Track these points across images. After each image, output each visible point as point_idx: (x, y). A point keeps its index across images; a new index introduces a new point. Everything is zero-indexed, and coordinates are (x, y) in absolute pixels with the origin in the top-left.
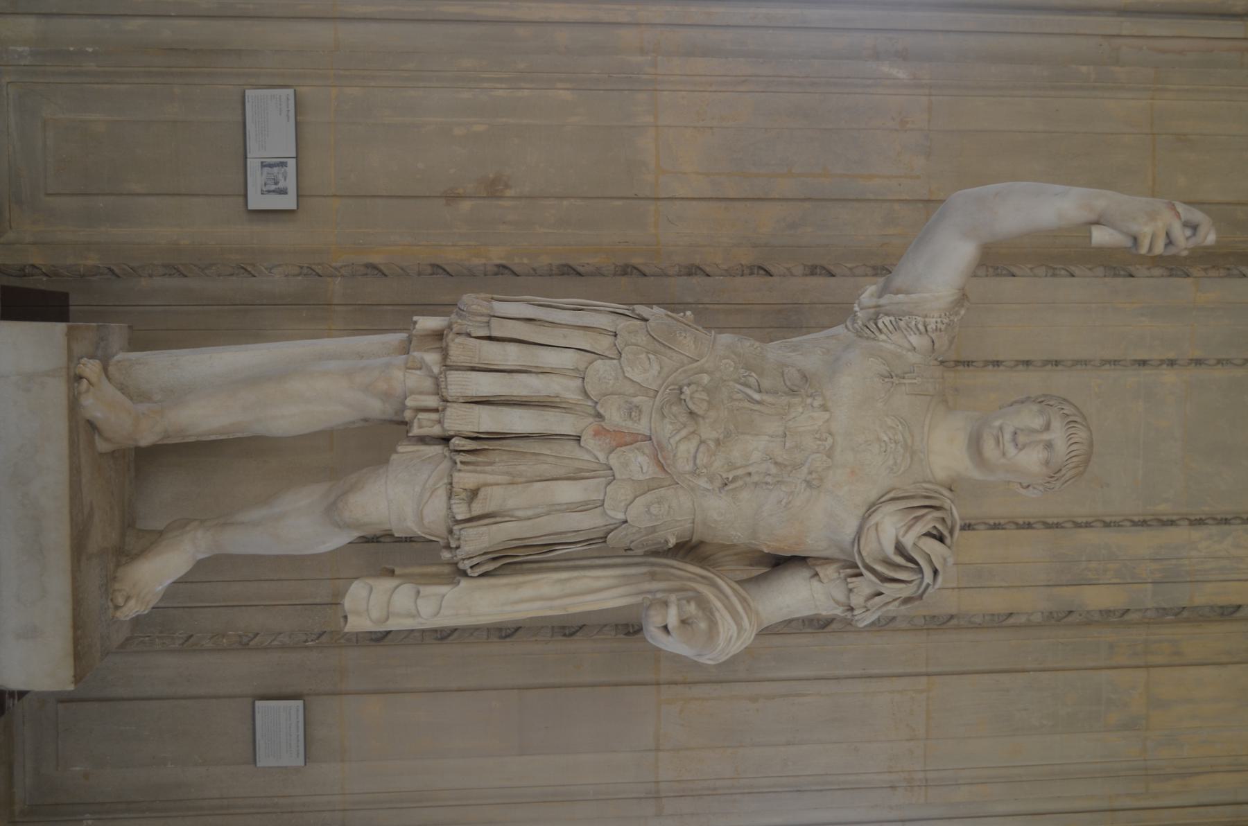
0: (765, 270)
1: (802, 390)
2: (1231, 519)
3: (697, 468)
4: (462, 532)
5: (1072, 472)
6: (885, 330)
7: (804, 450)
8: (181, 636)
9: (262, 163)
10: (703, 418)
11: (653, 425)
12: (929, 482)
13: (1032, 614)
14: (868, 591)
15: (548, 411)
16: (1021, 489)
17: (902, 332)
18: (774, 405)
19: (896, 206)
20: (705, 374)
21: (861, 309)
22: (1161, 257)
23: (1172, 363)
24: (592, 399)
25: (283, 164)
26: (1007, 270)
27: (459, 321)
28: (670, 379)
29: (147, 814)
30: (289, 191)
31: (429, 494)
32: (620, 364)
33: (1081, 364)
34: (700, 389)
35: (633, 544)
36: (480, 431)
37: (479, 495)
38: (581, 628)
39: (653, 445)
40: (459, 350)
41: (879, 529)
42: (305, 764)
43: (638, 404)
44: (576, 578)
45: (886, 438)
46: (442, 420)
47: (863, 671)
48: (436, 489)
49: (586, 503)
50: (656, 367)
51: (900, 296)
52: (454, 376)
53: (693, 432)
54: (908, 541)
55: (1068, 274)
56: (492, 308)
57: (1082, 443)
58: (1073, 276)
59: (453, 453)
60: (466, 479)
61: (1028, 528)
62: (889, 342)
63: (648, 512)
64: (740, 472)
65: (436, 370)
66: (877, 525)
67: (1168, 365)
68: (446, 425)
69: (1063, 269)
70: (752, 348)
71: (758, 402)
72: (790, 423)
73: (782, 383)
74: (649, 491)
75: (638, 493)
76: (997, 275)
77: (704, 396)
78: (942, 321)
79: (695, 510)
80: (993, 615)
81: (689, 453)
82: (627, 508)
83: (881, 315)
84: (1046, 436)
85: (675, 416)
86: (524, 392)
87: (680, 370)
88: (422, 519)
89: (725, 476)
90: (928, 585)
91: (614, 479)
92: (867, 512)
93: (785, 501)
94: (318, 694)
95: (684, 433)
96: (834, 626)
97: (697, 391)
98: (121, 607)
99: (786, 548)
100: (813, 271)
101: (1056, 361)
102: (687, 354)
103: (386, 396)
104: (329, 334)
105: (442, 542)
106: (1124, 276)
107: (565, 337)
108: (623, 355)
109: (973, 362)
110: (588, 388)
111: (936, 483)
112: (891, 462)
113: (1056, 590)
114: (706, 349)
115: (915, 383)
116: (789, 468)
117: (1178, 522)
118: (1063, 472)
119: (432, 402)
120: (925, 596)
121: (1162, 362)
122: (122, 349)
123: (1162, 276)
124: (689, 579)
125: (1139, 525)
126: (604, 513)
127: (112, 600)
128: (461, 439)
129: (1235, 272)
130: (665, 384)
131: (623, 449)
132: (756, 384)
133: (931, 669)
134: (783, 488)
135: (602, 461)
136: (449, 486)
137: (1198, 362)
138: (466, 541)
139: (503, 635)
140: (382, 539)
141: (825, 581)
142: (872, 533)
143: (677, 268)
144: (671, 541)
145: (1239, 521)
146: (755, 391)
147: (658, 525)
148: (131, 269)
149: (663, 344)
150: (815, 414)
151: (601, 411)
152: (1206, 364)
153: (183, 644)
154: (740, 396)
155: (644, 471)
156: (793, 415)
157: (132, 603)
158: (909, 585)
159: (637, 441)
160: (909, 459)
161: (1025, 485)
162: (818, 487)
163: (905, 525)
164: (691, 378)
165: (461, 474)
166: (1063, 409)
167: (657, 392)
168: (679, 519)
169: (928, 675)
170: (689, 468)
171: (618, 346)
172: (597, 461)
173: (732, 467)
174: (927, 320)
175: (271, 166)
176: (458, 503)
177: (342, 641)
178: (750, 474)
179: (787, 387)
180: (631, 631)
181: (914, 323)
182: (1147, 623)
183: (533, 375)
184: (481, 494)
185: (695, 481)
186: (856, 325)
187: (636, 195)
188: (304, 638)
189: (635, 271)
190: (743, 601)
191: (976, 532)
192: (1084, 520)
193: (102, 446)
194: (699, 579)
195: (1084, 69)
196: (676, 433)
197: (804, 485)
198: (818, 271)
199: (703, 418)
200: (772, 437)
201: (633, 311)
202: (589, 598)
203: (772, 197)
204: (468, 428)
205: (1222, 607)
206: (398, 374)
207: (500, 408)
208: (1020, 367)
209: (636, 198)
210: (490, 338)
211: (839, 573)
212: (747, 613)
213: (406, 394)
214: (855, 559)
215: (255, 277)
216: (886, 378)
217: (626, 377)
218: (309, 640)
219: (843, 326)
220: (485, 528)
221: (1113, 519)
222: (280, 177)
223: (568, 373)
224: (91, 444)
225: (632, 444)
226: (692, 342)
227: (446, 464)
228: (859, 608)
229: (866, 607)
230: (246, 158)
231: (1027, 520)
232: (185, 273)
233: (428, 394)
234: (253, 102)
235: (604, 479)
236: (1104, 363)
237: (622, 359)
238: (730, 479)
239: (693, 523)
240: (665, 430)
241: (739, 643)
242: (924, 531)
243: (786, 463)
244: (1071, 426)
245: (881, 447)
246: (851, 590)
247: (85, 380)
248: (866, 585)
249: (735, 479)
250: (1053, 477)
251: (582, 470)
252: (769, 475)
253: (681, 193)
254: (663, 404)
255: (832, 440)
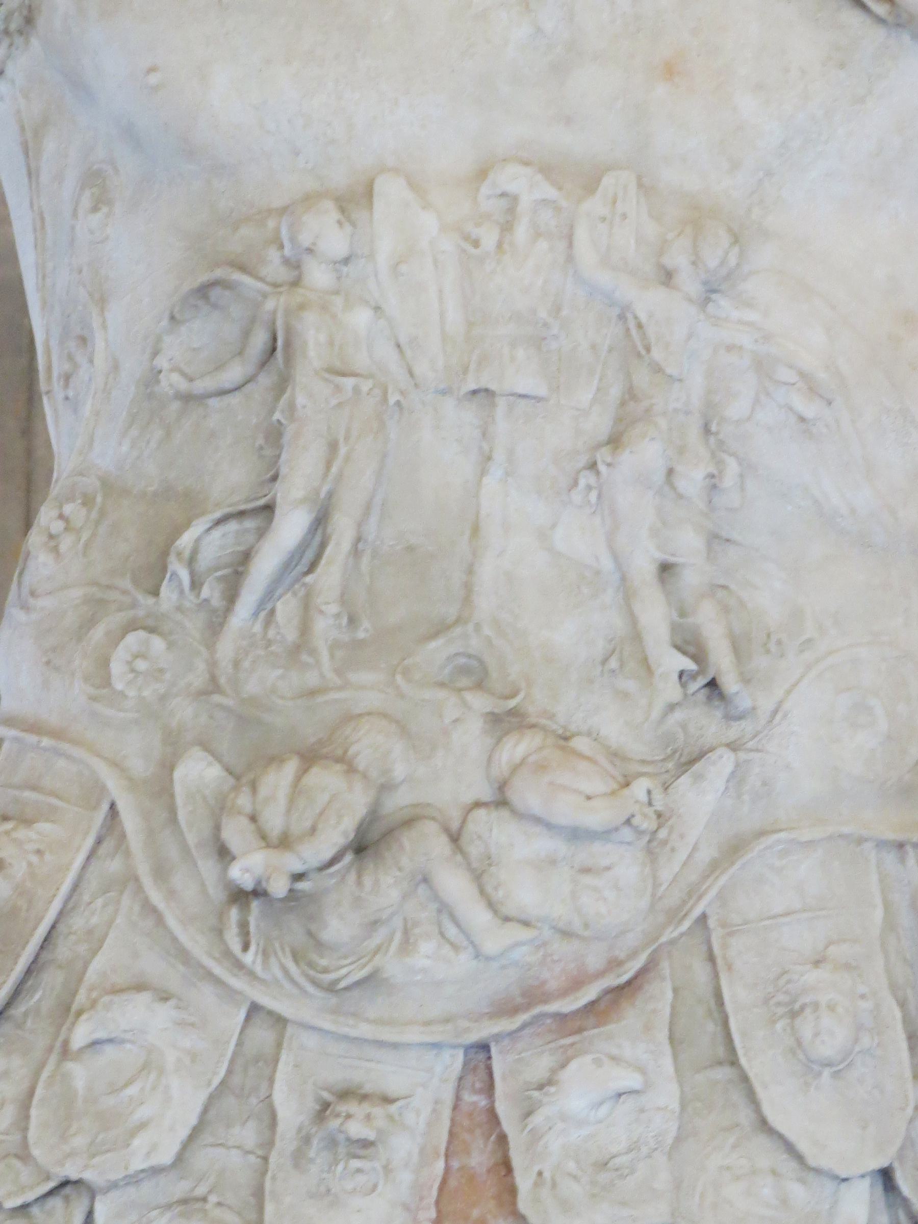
1: (270, 305)
7: (557, 309)
10: (386, 788)
11: (413, 1035)
18: (333, 447)
20: (178, 774)
32: (114, 1186)
34: (244, 801)
39: (512, 1035)
43: (312, 1106)
53: (455, 838)
70: (66, 544)
72: (422, 368)
73: (234, 400)
74: (734, 1062)
75: (745, 1116)
79: (830, 838)
81: (553, 862)
82: (818, 1171)
87: (156, 897)
89: (671, 691)
93: (801, 404)
104: (38, 379)
108: (71, 1171)
114: (61, 763)
116: (642, 378)
130: (218, 970)
131: (524, 1182)
132: (232, 526)
134: (737, 409)
146: (262, 533)
149: (29, 972)
156: (385, 352)
164: (191, 839)
167: (254, 1009)
168: (878, 914)
171: (30, 1196)
178: (666, 569)
197: (723, 305)
217: (180, 1159)
225: (503, 1139)
226: (22, 833)
238: (690, 665)
243: (615, 392)
254: (315, 983)
255: (513, 169)
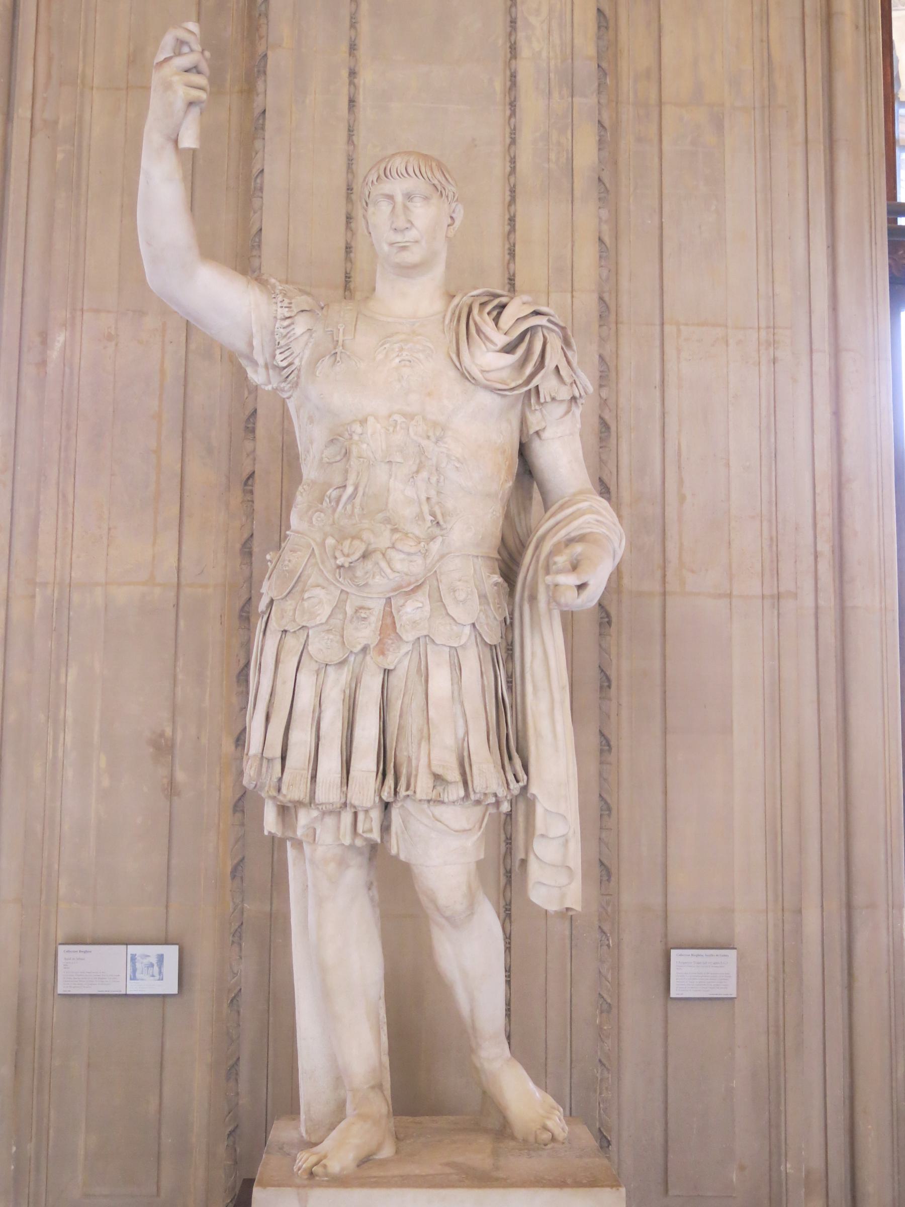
0: (248, 479)
2: (511, 17)
3: (420, 551)
4: (477, 791)
5: (438, 175)
6: (290, 360)
8: (599, 1071)
9: (131, 979)
10: (369, 544)
12: (444, 318)
13: (600, 219)
14: (553, 382)
15: (358, 702)
16: (454, 225)
17: (291, 342)
18: (358, 473)
19: (193, 346)
21: (270, 383)
22: (211, 80)
23: (353, 73)
24: (348, 656)
25: (133, 958)
26: (255, 236)
27: (266, 788)
28: (330, 577)
29: (782, 1108)
30: (160, 953)
31: (439, 824)
33: (352, 164)
34: (340, 547)
35: (497, 617)
36: (375, 770)
37: (439, 773)
38: (602, 671)
40: (295, 790)
41: (487, 369)
42: (735, 949)
43: (354, 610)
44: (533, 676)
45: (397, 360)
46: (365, 809)
47: (657, 388)
48: (434, 816)
49: (452, 665)
50: (318, 591)
51: (255, 343)
52: (320, 796)
53: (384, 555)
54: (501, 340)
55: (261, 175)
56: (255, 755)
57: (407, 163)
58: (262, 171)
59: (398, 798)
60: (423, 785)
61: (514, 221)
62: (302, 353)
63: (464, 602)
64: (426, 509)
65: (315, 813)
66: (483, 371)
67: (355, 78)
68: (369, 804)
69: (255, 181)
70: (304, 494)
71: (356, 489)
73: (338, 464)
75: (444, 612)
76: (259, 246)
77: (347, 543)
78: (281, 302)
80: (600, 257)
82: (459, 624)
83: (275, 363)
84: (399, 199)
85: (367, 573)
86: (339, 725)
87: (322, 567)
88: (465, 831)
89: (429, 524)
90: (549, 321)
91: (428, 636)
92: (470, 381)
94: (666, 936)
95: (383, 564)
96: (607, 417)
97: (342, 551)
98: (553, 1136)
99: (507, 463)
100: (250, 430)
101: (348, 189)
102: (306, 559)
103: (342, 863)
105: (492, 810)
106: (264, 119)
107: (284, 683)
108: (304, 624)
109: (346, 273)
110: (337, 660)
111: (446, 311)
112: (421, 356)
113: (577, 194)
115: (344, 329)
117: (513, 71)
118: (436, 182)
119: (347, 818)
120: (562, 324)
121: (351, 83)
122: (297, 1128)
123: (265, 81)
124: (537, 561)
125: (515, 110)
126: (463, 647)
127: (545, 1145)
128: (383, 789)
129: (263, 8)
131: (398, 626)
132: (338, 490)
133: (657, 322)
134: (443, 465)
135: (410, 648)
136: (431, 803)
137: (353, 47)
138: (487, 787)
139: (607, 748)
140: (508, 867)
141: (543, 424)
142: (492, 376)
143: (244, 567)
144: (496, 579)
145: (513, 10)
147: (478, 593)
148: (229, 1113)
150: (370, 432)
151: (359, 647)
152: (355, 39)
153: (608, 1070)
154: (349, 507)
155: (421, 605)
157: (550, 1124)
158: (548, 340)
159: (392, 612)
160: (419, 337)
161: (450, 221)
162: (443, 430)
163: (484, 344)
165: (418, 791)
166: (372, 181)
167: (342, 591)
169: (662, 324)
170: (419, 560)
171: (296, 629)
172: (411, 652)
173: (420, 517)
174: (279, 317)
175: (134, 971)
176: (448, 795)
177: (609, 909)
178: (428, 499)
179: (342, 459)
180: (606, 620)
181: (282, 330)
182: (617, 103)
183: (322, 715)
184: (439, 771)
185: (433, 554)
186: (286, 389)
187: (174, 606)
188: (605, 947)
189: (246, 609)
190: (562, 508)
191: (516, 272)
192: (508, 164)
193: (387, 1151)
194: (538, 551)
195: (60, 156)
196: (384, 572)
198: (250, 425)
199: (369, 544)
200: (391, 475)
201: (263, 613)
202: (552, 663)
203: (180, 470)
204: (372, 782)
205: (599, 27)
206: (320, 851)
207: (354, 750)
208: (353, 225)
209: (177, 605)
210: (283, 758)
211: (536, 410)
212: (575, 504)
213: (339, 845)
214: (521, 394)
215: (241, 989)
216: (336, 359)
218: (607, 942)
219: (287, 401)
220: (474, 767)
221: (507, 135)
222: (146, 961)
223: (320, 681)
224: (383, 1163)
225: (394, 617)
227: (409, 804)
228: (573, 391)
229: (571, 384)
230: (126, 995)
231: (507, 222)
232: (235, 1059)
233: (339, 821)
234: (70, 987)
235: (428, 646)
236: (350, 142)
237: (307, 625)
239: (477, 556)
240: (381, 583)
241: (604, 513)
242: (492, 324)
243: (418, 462)
244: (389, 174)
245: (405, 366)
246: (553, 399)
247: (313, 1169)
248: (547, 383)
249: (433, 515)
250: (441, 192)
251: (419, 670)
252: (429, 478)
253: (172, 561)
254: (355, 585)
255: (396, 415)
